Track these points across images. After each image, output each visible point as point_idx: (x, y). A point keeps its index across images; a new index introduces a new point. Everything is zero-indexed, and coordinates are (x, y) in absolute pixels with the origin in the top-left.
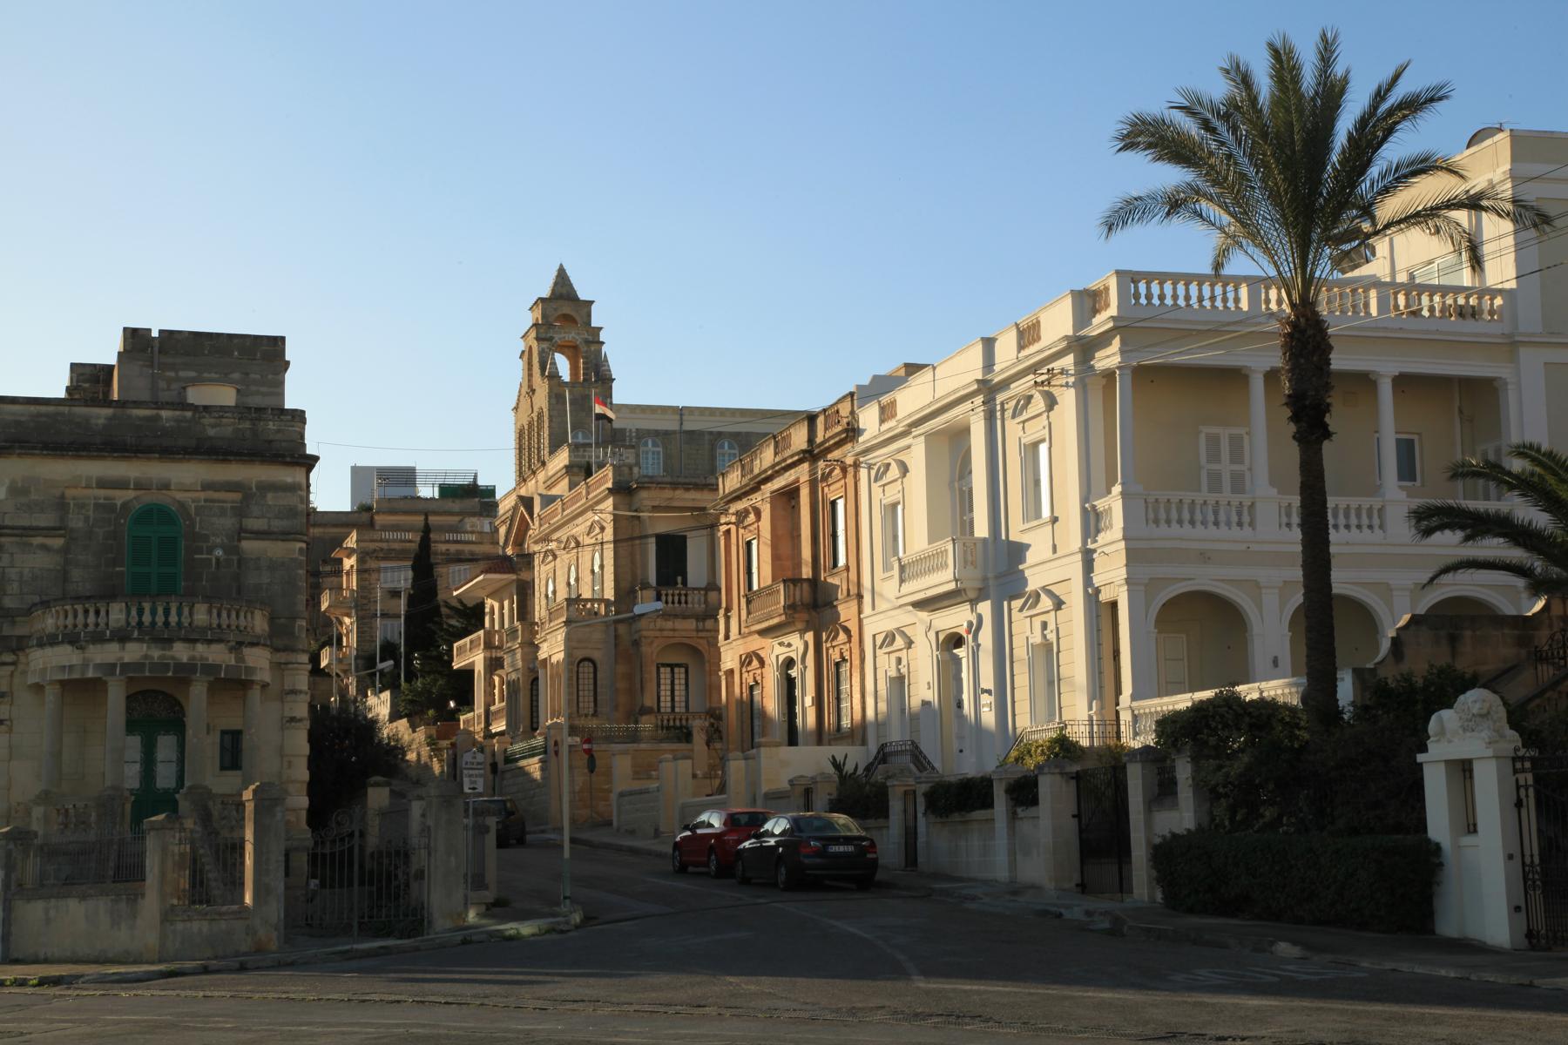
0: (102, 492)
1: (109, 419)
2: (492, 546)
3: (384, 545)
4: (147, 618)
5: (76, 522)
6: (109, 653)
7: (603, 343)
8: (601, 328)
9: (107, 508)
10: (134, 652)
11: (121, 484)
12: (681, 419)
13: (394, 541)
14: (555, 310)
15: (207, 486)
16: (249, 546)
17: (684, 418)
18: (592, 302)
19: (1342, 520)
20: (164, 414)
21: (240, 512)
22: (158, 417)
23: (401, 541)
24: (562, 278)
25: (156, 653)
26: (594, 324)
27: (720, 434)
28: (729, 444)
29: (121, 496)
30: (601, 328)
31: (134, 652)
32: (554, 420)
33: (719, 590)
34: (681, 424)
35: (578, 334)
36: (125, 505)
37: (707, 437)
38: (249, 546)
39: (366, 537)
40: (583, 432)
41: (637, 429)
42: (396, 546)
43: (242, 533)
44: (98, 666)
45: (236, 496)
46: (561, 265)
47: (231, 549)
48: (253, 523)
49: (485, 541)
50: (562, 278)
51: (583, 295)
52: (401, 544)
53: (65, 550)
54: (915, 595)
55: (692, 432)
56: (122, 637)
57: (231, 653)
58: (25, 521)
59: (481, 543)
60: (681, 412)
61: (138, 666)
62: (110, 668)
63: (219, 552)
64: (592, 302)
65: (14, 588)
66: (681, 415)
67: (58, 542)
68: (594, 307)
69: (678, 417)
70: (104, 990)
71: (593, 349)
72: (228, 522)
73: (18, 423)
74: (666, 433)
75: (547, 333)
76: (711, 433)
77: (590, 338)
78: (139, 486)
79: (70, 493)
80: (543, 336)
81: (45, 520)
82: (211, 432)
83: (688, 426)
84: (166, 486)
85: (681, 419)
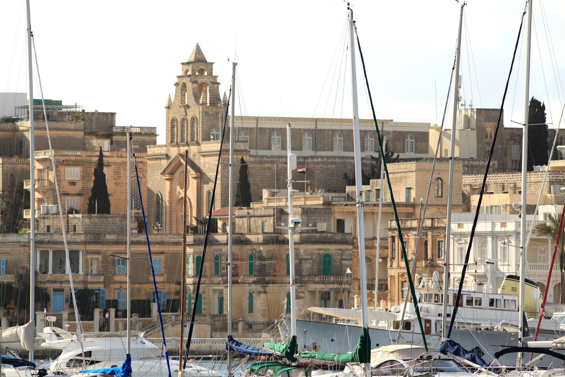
0: (318, 251)
1: (320, 236)
2: (117, 159)
3: (67, 158)
4: (337, 279)
5: (314, 257)
6: (331, 286)
7: (219, 84)
8: (217, 76)
9: (319, 254)
10: (336, 286)
11: (321, 250)
12: (257, 123)
13: (72, 156)
14: (198, 67)
15: (336, 250)
16: (343, 262)
17: (259, 122)
18: (213, 63)
19: (555, 268)
20: (329, 235)
21: (342, 255)
22: (327, 236)
23: (75, 156)
24: (198, 50)
25: (339, 286)
26: (214, 74)
27: (273, 129)
28: (277, 133)
29: (321, 252)
30: (217, 76)
31: (336, 286)
32: (204, 123)
33: (357, 239)
34: (257, 125)
35: (208, 79)
36: (322, 254)
37: (268, 131)
38: (343, 262)
39: (59, 154)
40: (216, 129)
41: (238, 127)
42: (73, 158)
43: (342, 259)
44: (329, 289)
45: (341, 252)
46: (197, 43)
47: (340, 263)
48: (344, 257)
49: (114, 155)
50: (198, 50)
51: (209, 60)
52: (76, 157)
53: (312, 263)
54: (452, 259)
55: (261, 129)
56: (333, 283)
57: (86, 233)
58: (306, 257)
59: (112, 157)
60: (257, 119)
61: (336, 289)
62: (331, 289)
63: (338, 263)
64: (213, 63)
65: (304, 271)
66: (257, 121)
67: (311, 262)
68: (214, 65)
69: (256, 122)
70: (408, 343)
71: (215, 86)
72: (339, 257)
73: (305, 237)
74: (251, 129)
75: (194, 79)
76: (269, 129)
77: (213, 81)
78: (325, 250)
79: (313, 251)
80: (193, 80)
81: (309, 257)
82: (337, 238)
83: (260, 126)
84: (329, 250)
85: (257, 123)
